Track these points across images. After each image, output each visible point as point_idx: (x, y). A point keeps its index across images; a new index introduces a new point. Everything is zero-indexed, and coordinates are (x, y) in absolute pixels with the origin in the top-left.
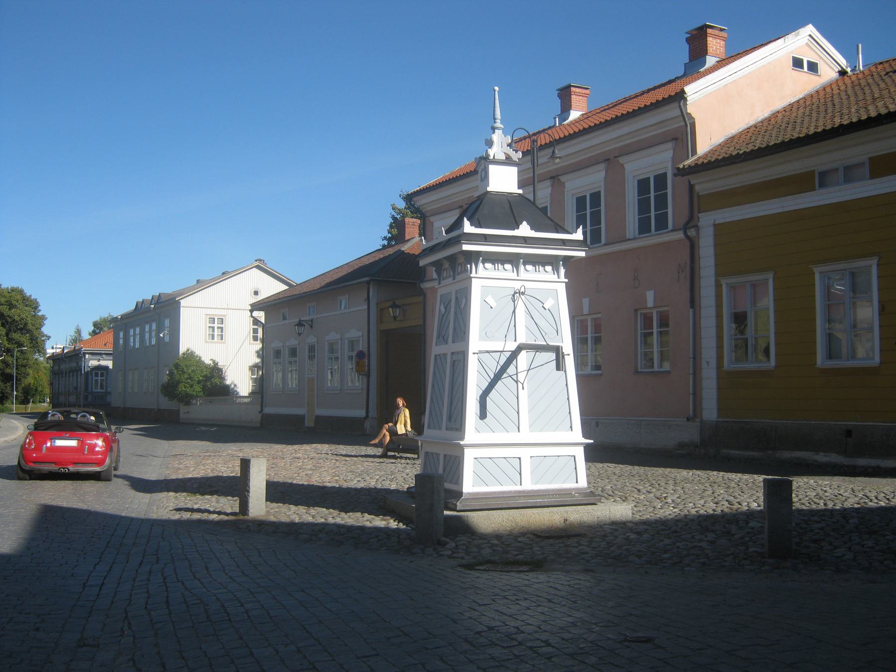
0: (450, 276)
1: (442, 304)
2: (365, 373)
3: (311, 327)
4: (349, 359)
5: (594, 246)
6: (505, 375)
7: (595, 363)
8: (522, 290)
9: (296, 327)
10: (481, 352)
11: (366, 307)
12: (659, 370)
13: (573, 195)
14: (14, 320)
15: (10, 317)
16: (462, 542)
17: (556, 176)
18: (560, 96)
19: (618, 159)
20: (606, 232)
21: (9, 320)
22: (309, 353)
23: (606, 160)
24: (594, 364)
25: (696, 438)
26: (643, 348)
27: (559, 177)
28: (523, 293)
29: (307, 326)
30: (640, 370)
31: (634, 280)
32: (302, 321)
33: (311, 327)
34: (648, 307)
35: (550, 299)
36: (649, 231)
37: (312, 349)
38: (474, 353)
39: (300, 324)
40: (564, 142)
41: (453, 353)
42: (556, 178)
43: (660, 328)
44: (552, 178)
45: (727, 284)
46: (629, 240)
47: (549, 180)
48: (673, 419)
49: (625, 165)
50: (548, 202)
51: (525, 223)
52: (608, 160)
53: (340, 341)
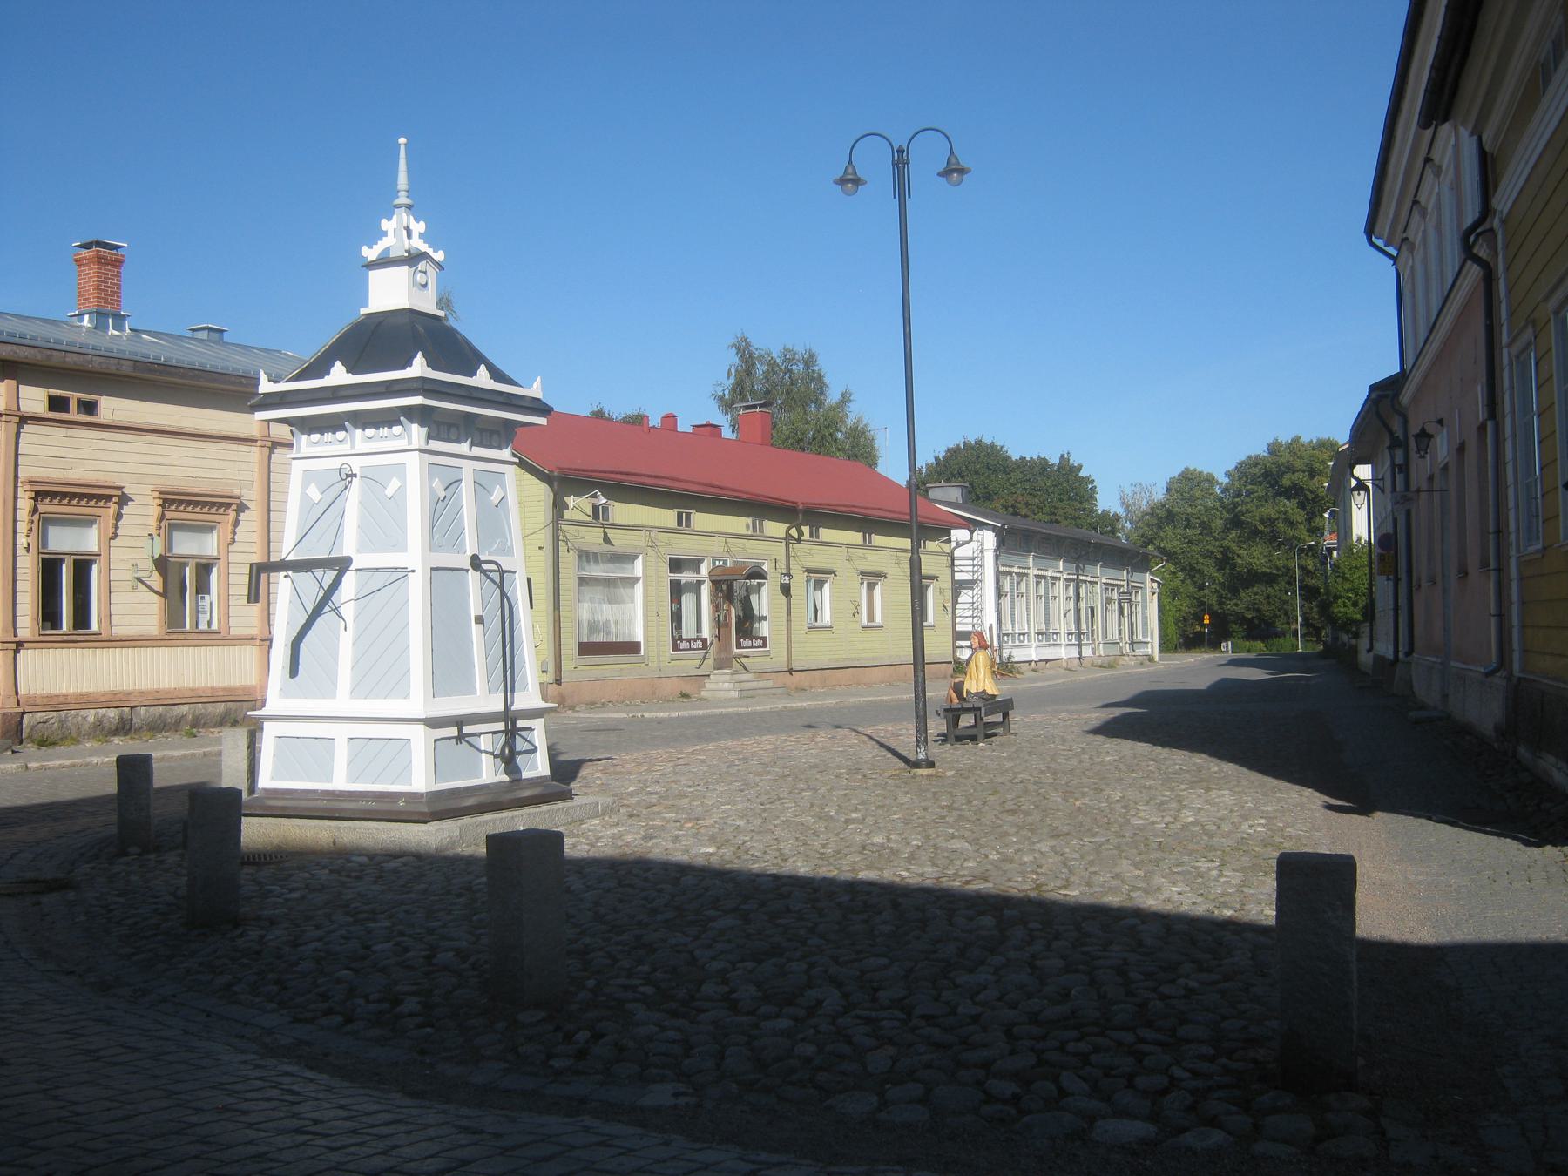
6: (327, 608)
14: (1317, 496)
15: (1311, 492)
21: (1310, 496)
51: (338, 364)
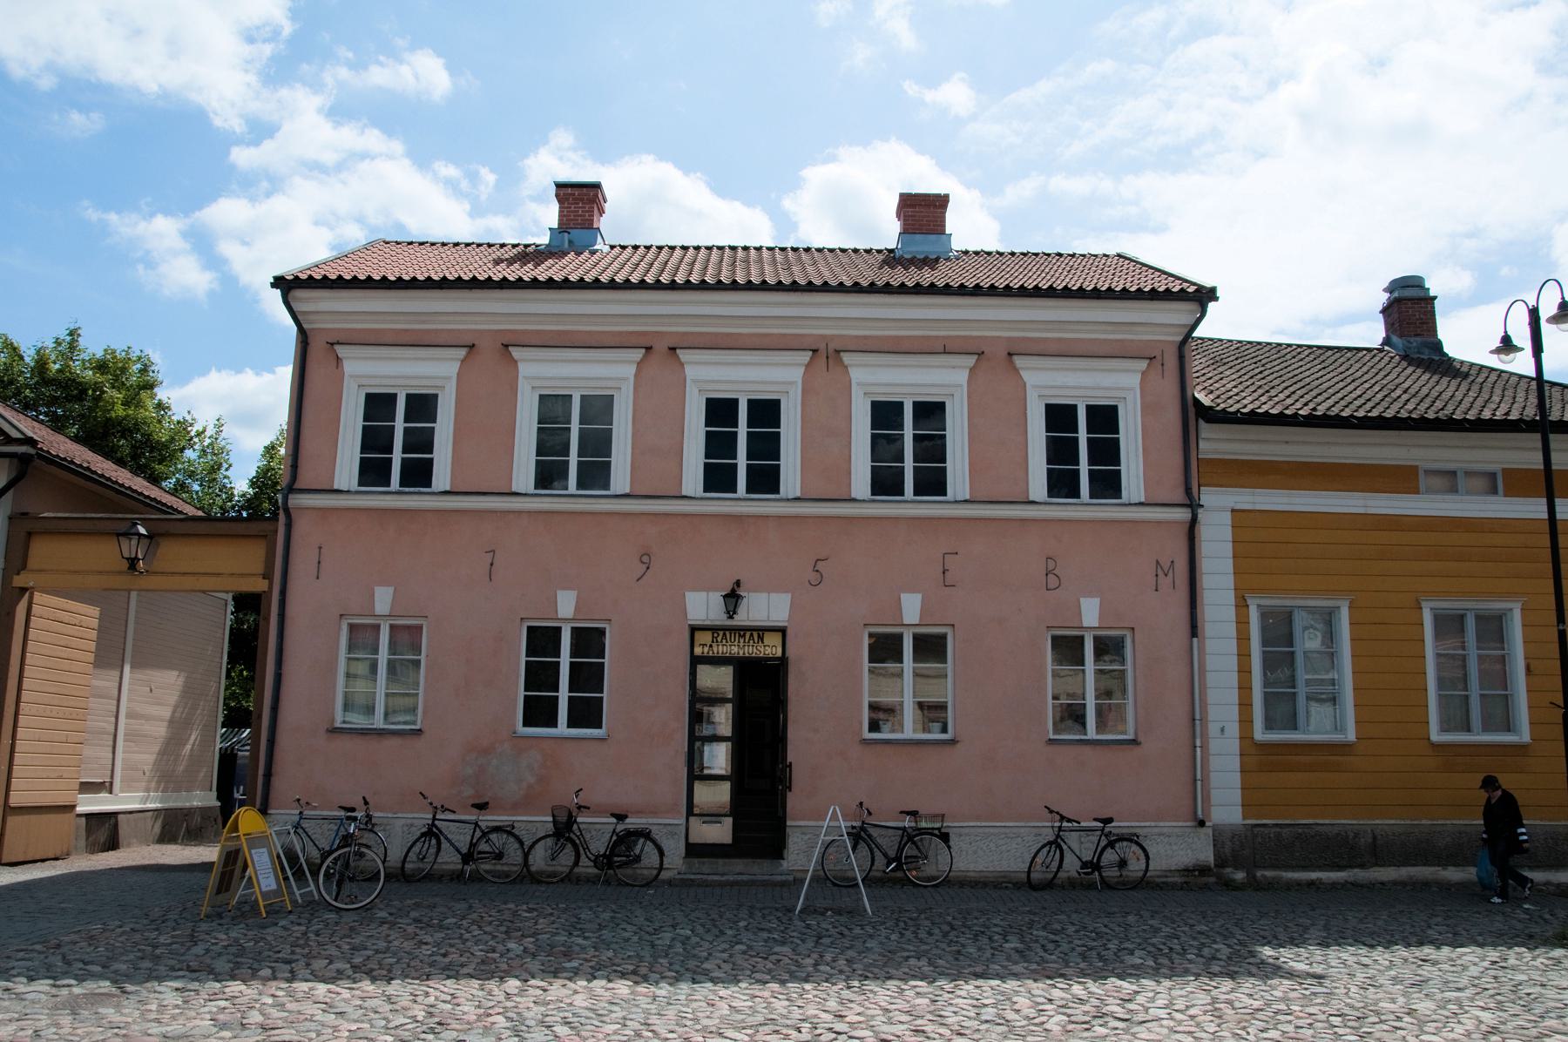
5: (407, 489)
12: (386, 727)
25: (1207, 856)
30: (338, 725)
34: (905, 623)
35: (904, 597)
45: (1259, 606)
46: (854, 500)
48: (1153, 824)
49: (519, 364)
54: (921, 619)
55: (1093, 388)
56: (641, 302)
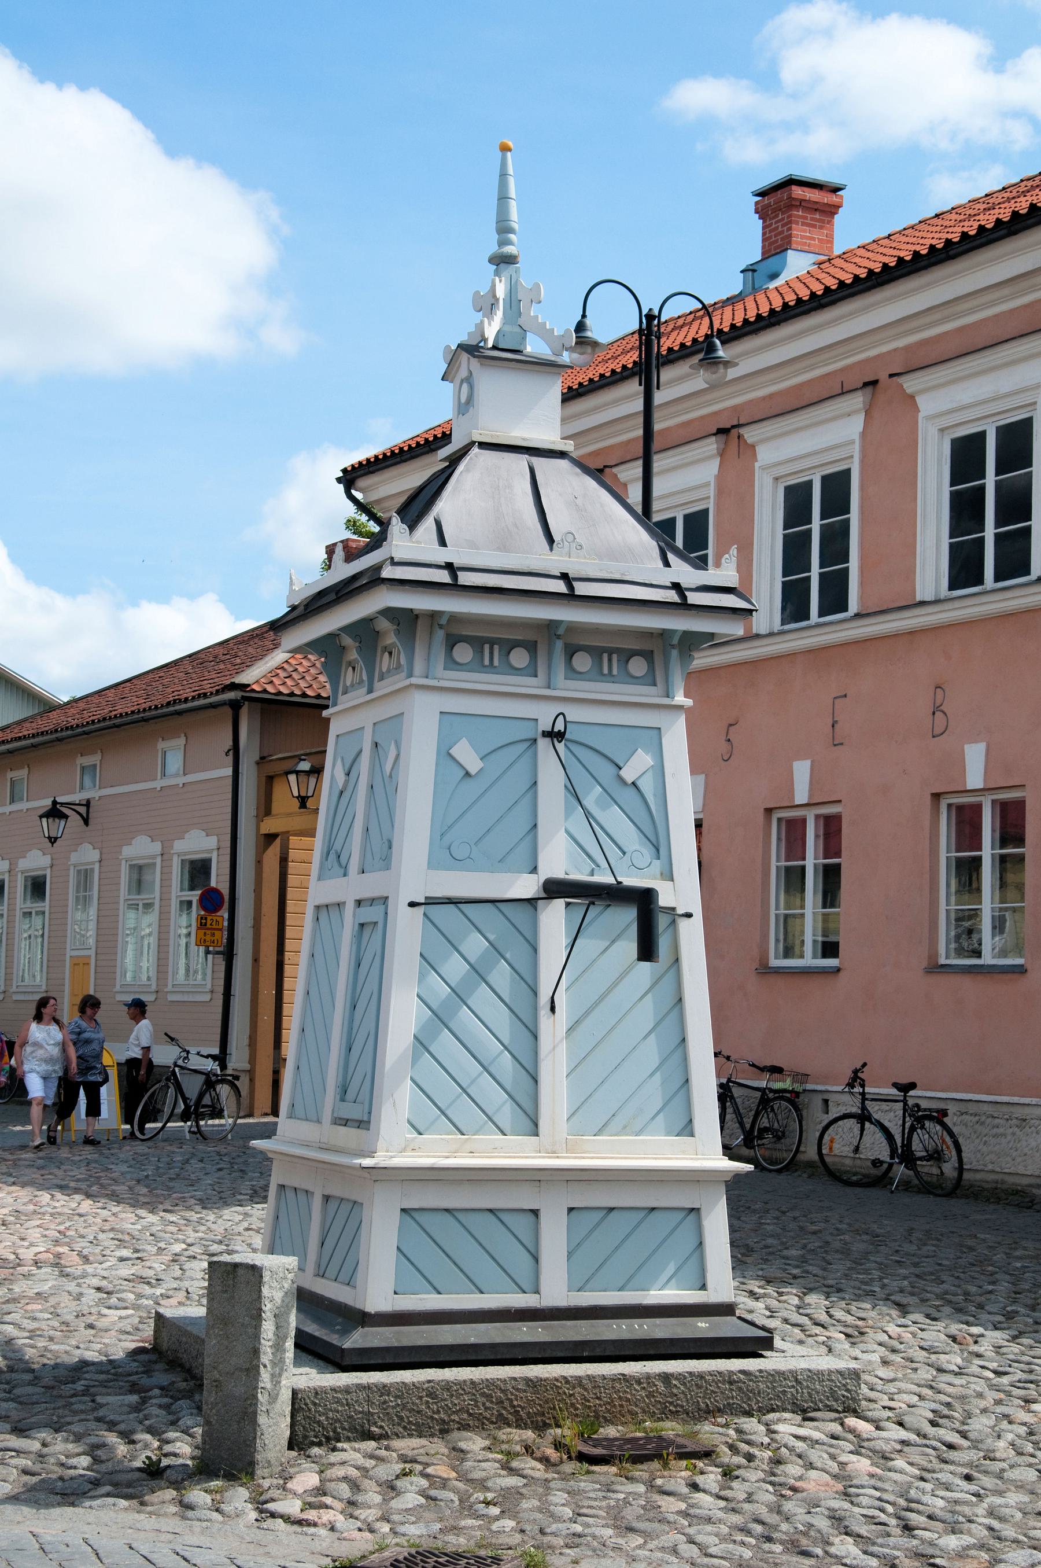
0: (361, 682)
1: (339, 762)
2: (221, 949)
3: (86, 821)
4: (181, 910)
7: (824, 936)
8: (560, 726)
9: (44, 820)
10: (430, 902)
11: (229, 771)
13: (776, 479)
16: (340, 1472)
17: (733, 427)
18: (762, 212)
19: (901, 380)
20: (862, 584)
22: (78, 891)
23: (866, 384)
24: (820, 939)
26: (953, 899)
27: (742, 431)
28: (560, 736)
29: (74, 820)
30: (943, 961)
31: (934, 713)
32: (62, 804)
33: (86, 821)
36: (979, 580)
37: (85, 876)
38: (412, 904)
39: (55, 812)
40: (756, 331)
41: (359, 903)
42: (734, 432)
43: (1002, 847)
44: (722, 431)
46: (922, 603)
47: (713, 439)
50: (708, 498)
52: (874, 383)
53: (158, 860)
54: (810, 796)
55: (994, 399)
56: (792, 338)
